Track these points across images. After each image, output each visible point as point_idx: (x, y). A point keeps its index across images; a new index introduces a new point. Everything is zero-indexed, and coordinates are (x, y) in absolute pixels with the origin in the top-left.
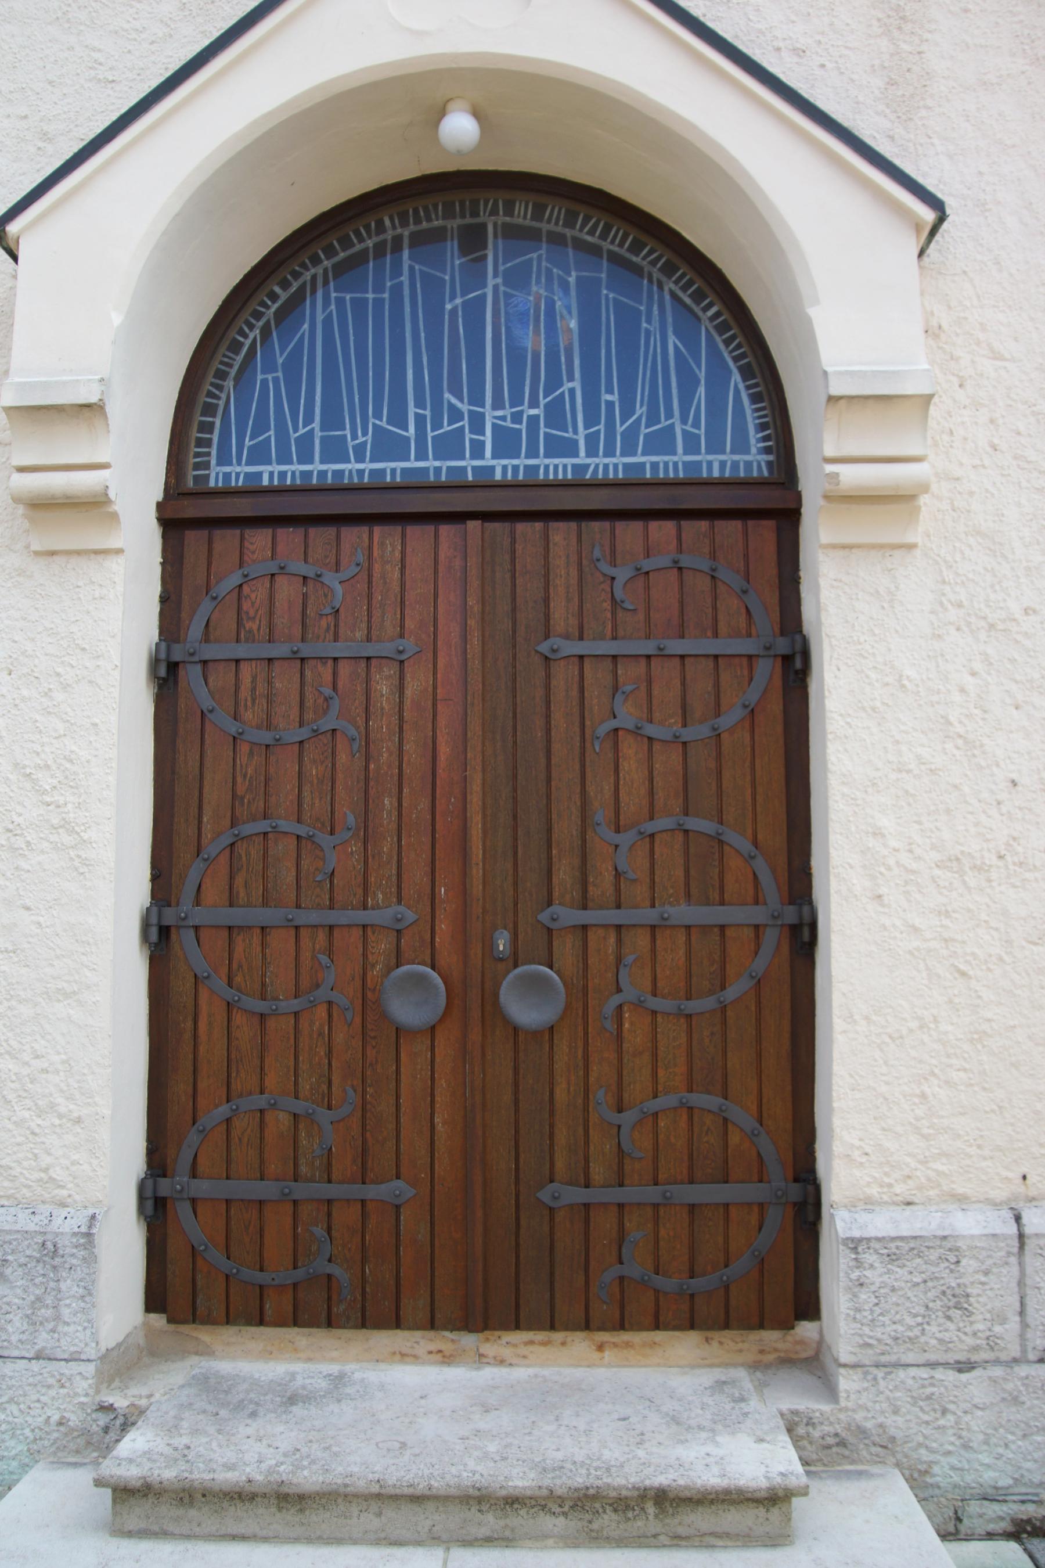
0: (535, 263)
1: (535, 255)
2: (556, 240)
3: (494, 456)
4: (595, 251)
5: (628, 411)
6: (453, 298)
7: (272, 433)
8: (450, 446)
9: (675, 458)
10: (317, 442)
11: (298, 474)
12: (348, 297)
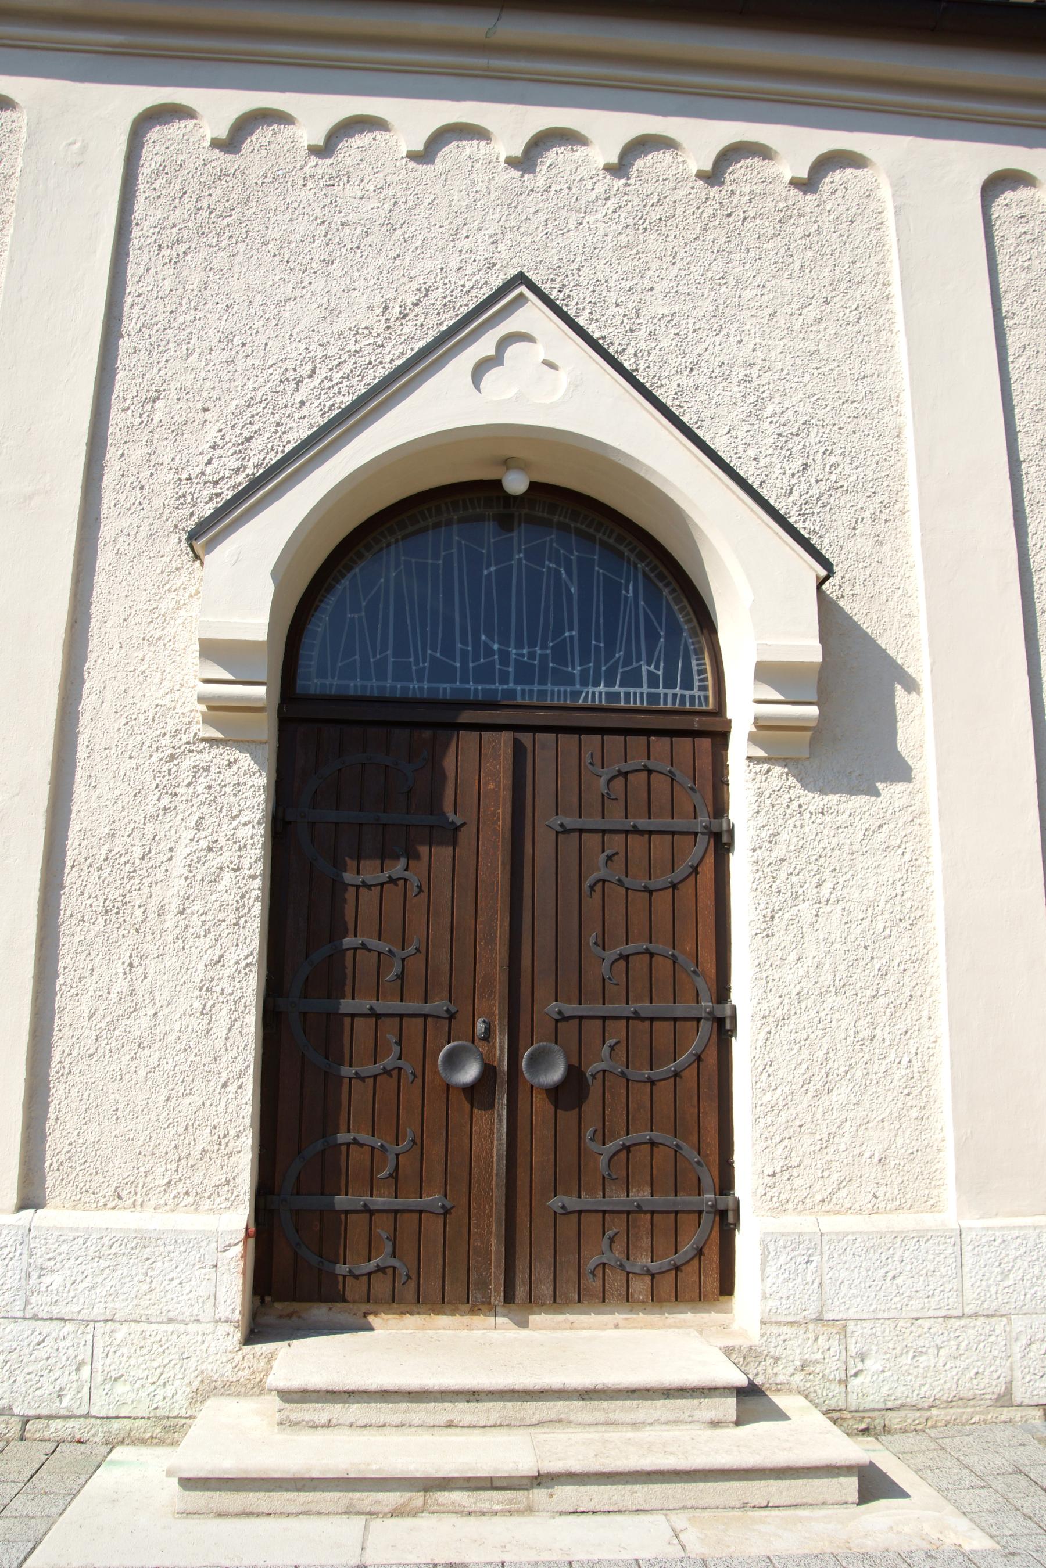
0: (548, 544)
1: (548, 539)
2: (563, 528)
3: (620, 686)
4: (591, 538)
5: (609, 654)
6: (489, 566)
7: (591, 664)
8: (485, 674)
9: (692, 692)
10: (390, 668)
11: (448, 691)
12: (413, 560)
